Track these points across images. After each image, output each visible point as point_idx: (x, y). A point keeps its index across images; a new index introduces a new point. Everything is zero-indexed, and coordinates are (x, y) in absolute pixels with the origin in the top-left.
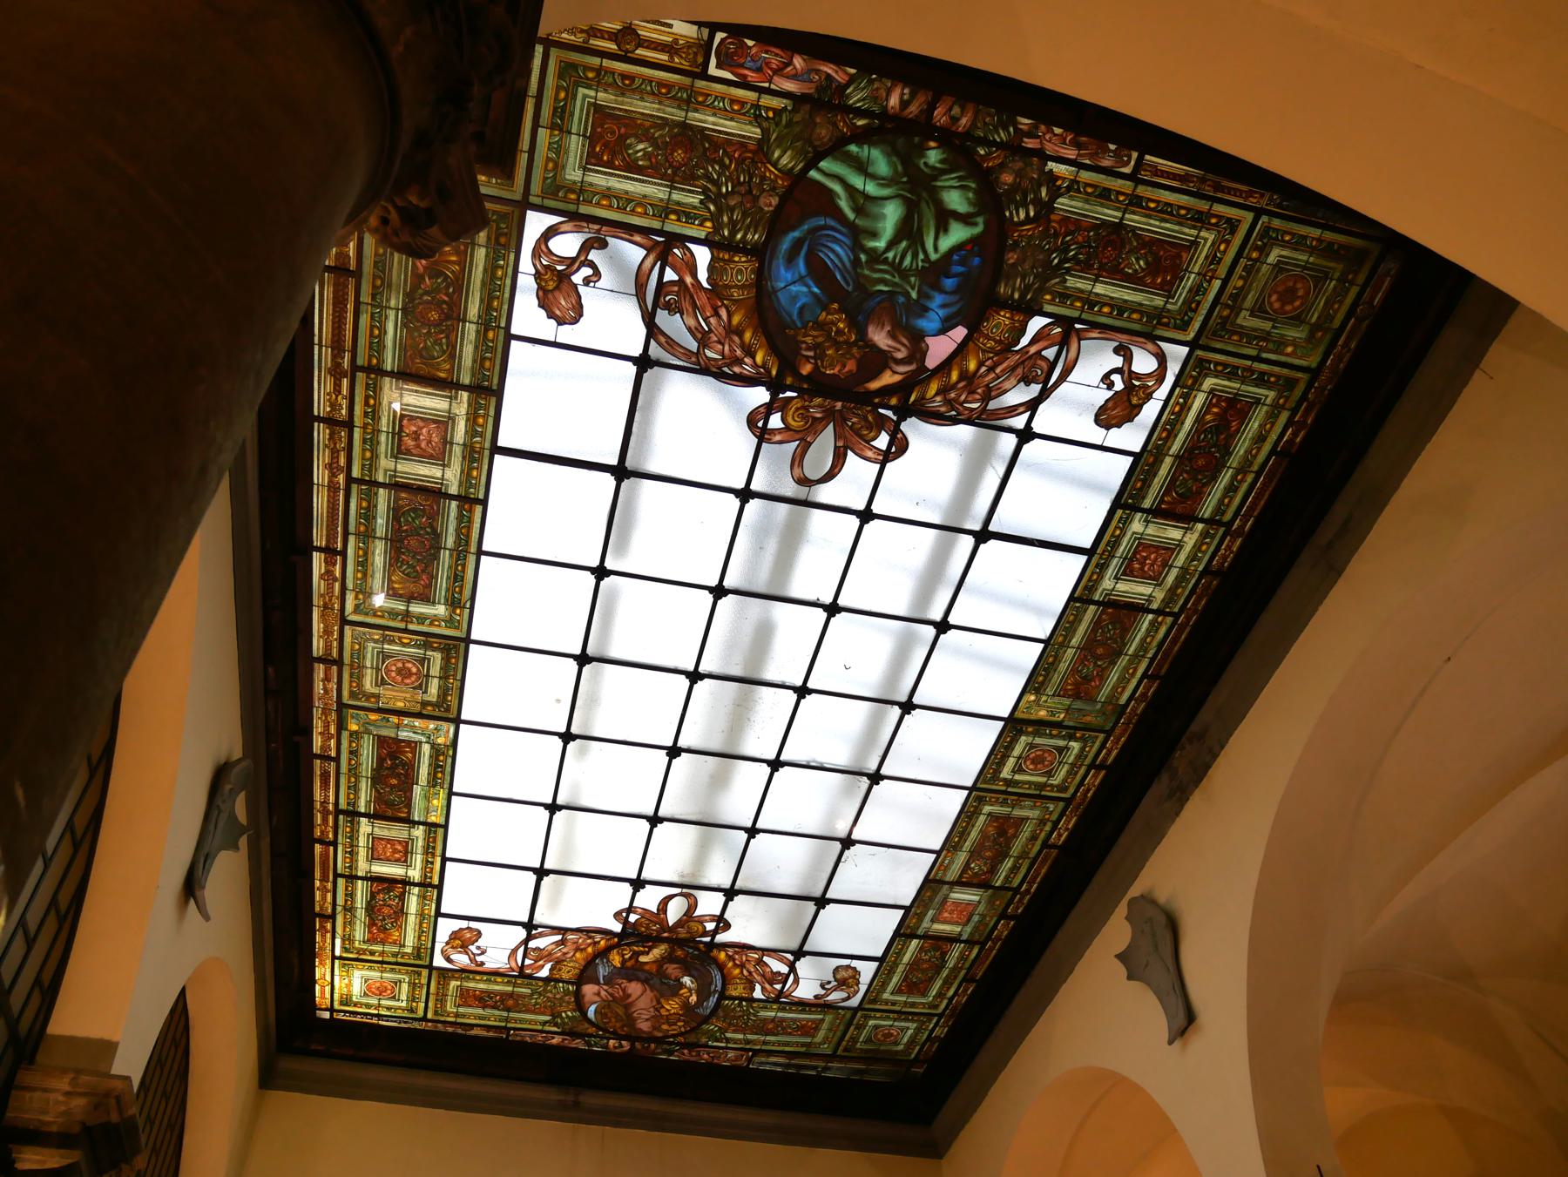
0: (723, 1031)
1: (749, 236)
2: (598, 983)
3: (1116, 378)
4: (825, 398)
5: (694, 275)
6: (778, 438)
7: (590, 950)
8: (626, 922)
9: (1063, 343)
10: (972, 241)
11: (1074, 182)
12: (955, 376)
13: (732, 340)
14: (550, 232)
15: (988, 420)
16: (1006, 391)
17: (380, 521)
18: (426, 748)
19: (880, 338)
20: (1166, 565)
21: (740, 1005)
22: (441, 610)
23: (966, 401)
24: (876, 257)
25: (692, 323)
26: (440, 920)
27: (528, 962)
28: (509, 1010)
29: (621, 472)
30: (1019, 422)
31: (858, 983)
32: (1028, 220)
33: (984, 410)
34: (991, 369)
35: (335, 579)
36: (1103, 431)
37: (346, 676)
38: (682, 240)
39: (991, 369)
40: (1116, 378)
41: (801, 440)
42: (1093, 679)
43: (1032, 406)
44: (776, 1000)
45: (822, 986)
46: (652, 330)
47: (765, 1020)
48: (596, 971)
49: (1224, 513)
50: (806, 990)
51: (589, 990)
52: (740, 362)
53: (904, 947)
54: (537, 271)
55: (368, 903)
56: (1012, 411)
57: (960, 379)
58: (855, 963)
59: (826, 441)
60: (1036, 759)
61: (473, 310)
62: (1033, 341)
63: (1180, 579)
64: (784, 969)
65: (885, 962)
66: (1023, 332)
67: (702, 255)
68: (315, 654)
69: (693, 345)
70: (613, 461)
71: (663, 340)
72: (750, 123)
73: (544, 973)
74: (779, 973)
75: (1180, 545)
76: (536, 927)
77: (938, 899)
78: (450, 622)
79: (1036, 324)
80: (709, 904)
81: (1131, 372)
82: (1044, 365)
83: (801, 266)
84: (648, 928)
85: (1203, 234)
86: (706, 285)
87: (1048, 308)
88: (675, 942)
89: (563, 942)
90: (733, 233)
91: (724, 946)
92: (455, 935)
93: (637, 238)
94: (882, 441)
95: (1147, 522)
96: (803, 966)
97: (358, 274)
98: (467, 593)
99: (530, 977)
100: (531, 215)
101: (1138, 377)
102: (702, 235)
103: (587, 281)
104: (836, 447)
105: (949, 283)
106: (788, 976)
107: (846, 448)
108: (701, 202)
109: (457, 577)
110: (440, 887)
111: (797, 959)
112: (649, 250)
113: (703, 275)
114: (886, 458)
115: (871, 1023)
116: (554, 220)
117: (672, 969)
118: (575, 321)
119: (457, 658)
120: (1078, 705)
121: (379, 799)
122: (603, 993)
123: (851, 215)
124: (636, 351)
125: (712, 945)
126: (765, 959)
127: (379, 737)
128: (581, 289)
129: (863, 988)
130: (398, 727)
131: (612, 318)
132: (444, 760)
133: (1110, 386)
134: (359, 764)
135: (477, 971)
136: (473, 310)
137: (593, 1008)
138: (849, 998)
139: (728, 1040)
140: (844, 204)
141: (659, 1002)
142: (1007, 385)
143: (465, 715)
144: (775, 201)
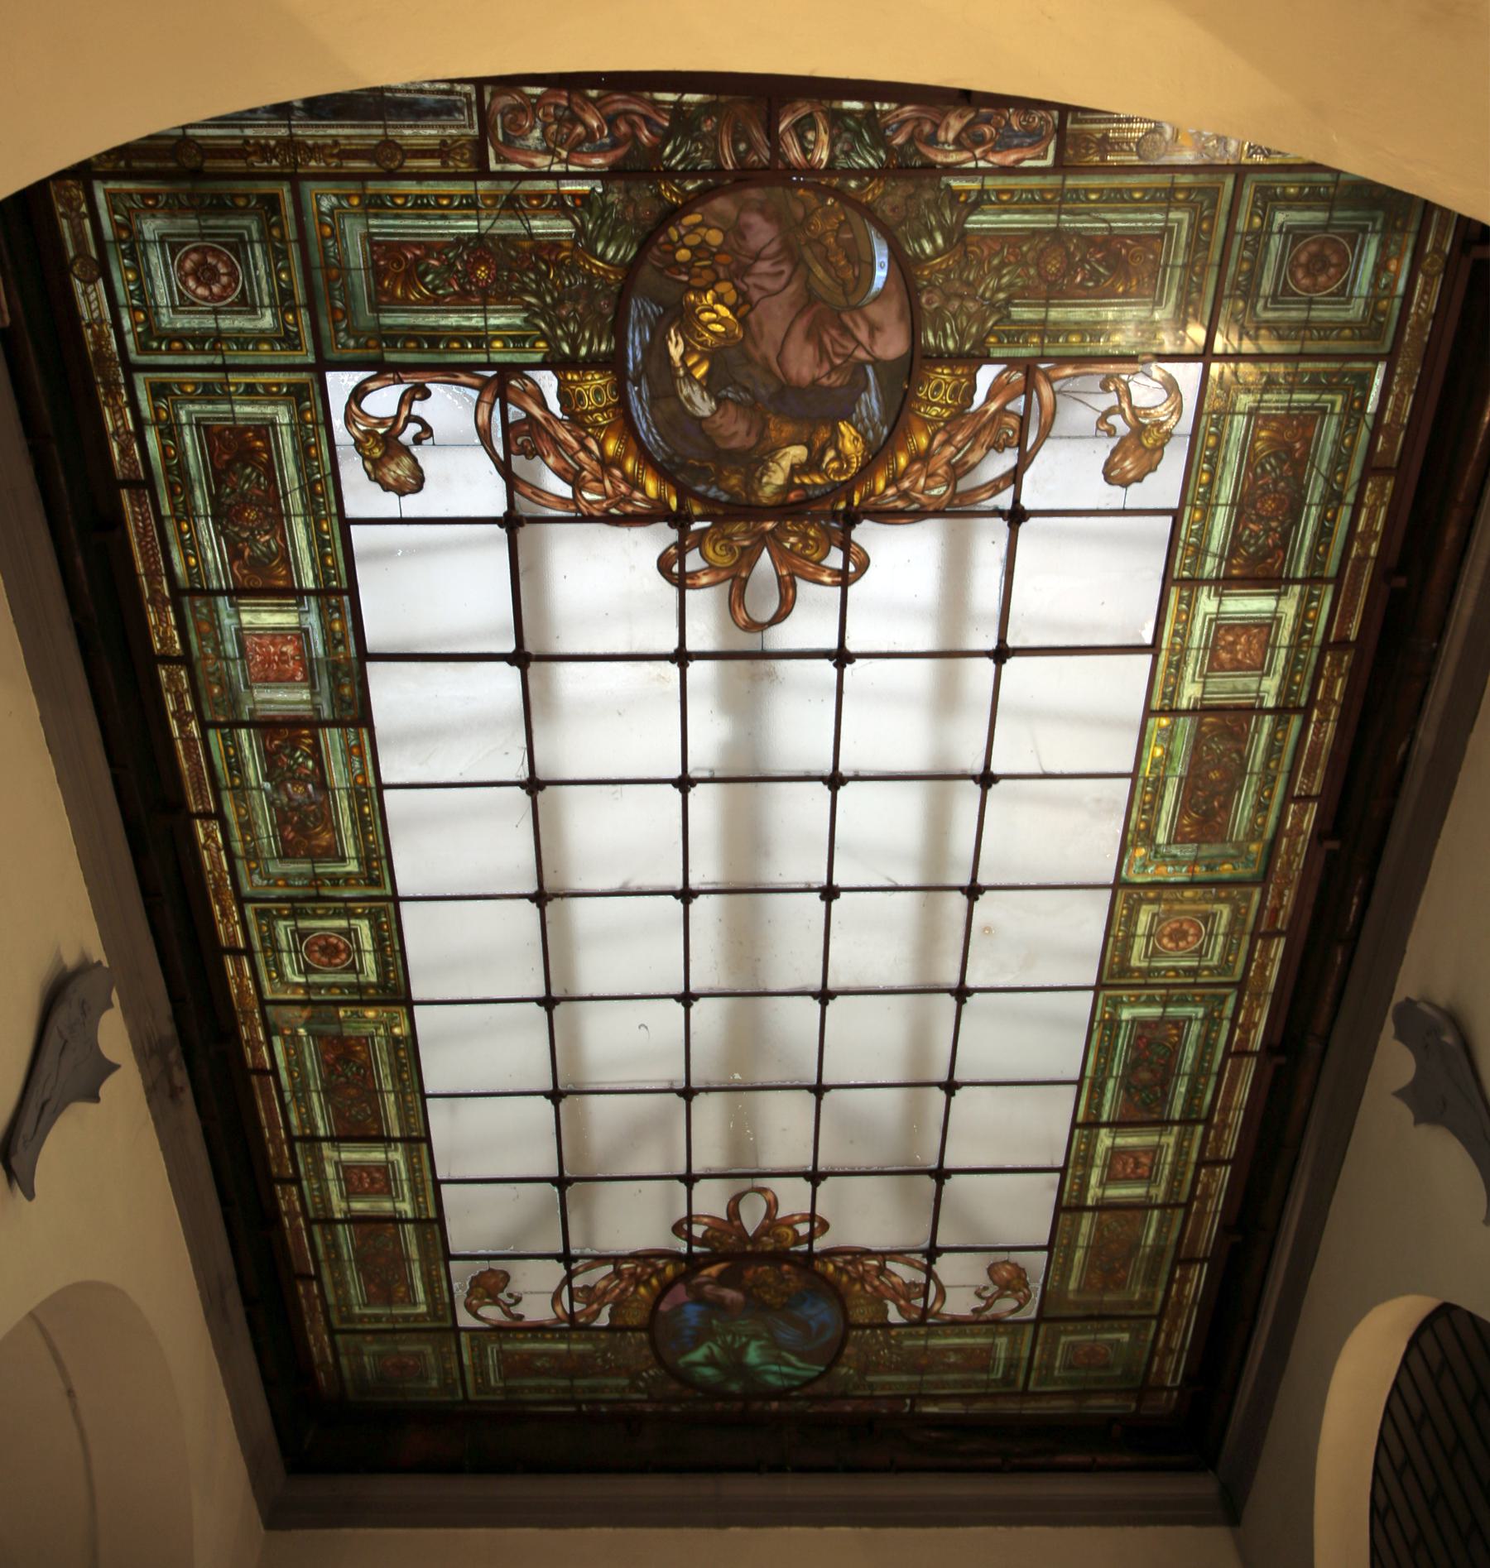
0: (583, 241)
2: (876, 362)
4: (748, 522)
5: (543, 404)
6: (704, 580)
7: (903, 461)
8: (846, 545)
9: (1029, 387)
10: (684, 1353)
13: (611, 475)
14: (359, 393)
15: (958, 508)
16: (974, 466)
17: (1183, 1090)
18: (1161, 837)
20: (1269, 645)
21: (875, 1336)
22: (1126, 1014)
25: (894, 1279)
26: (1175, 504)
30: (1004, 500)
32: (938, 253)
33: (954, 494)
35: (1242, 1026)
36: (1118, 489)
37: (1251, 919)
38: (518, 369)
40: (1115, 420)
42: (337, 1059)
43: (1015, 477)
44: (921, 1322)
45: (978, 1295)
49: (1323, 565)
51: (892, 345)
52: (847, 1262)
53: (1076, 1226)
54: (356, 439)
55: (1297, 521)
56: (995, 487)
57: (911, 462)
58: (1015, 1257)
60: (333, 951)
62: (990, 397)
63: (1292, 664)
64: (921, 1278)
65: (1057, 1244)
66: (973, 388)
67: (548, 382)
68: (1283, 941)
69: (566, 491)
70: (510, 647)
71: (528, 491)
74: (914, 1284)
75: (1276, 618)
76: (576, 1259)
78: (1117, 1003)
79: (986, 376)
80: (793, 1197)
81: (1133, 408)
82: (1014, 422)
83: (813, 1324)
84: (804, 537)
85: (1172, 215)
86: (560, 415)
87: (997, 353)
88: (743, 510)
89: (618, 1273)
90: (575, 348)
91: (830, 1253)
92: (476, 1282)
93: (463, 378)
95: (1220, 595)
96: (945, 1266)
97: (149, 483)
98: (1096, 1036)
99: (586, 1327)
100: (330, 376)
103: (418, 440)
105: (688, 1332)
106: (927, 1286)
107: (792, 575)
108: (526, 320)
109: (1106, 1052)
110: (1167, 580)
111: (932, 1261)
112: (481, 390)
113: (554, 406)
114: (844, 580)
116: (358, 376)
117: (736, 431)
119: (1112, 963)
120: (1207, 850)
121: (338, 1115)
122: (862, 335)
123: (784, 1354)
124: (499, 508)
125: (810, 1255)
126: (890, 1265)
127: (1223, 841)
130: (1196, 861)
132: (407, 1052)
133: (1111, 431)
134: (1259, 792)
135: (517, 1328)
138: (1020, 1307)
139: (871, 1386)
140: (793, 1359)
141: (743, 321)
143: (416, 994)
144: (847, 1351)
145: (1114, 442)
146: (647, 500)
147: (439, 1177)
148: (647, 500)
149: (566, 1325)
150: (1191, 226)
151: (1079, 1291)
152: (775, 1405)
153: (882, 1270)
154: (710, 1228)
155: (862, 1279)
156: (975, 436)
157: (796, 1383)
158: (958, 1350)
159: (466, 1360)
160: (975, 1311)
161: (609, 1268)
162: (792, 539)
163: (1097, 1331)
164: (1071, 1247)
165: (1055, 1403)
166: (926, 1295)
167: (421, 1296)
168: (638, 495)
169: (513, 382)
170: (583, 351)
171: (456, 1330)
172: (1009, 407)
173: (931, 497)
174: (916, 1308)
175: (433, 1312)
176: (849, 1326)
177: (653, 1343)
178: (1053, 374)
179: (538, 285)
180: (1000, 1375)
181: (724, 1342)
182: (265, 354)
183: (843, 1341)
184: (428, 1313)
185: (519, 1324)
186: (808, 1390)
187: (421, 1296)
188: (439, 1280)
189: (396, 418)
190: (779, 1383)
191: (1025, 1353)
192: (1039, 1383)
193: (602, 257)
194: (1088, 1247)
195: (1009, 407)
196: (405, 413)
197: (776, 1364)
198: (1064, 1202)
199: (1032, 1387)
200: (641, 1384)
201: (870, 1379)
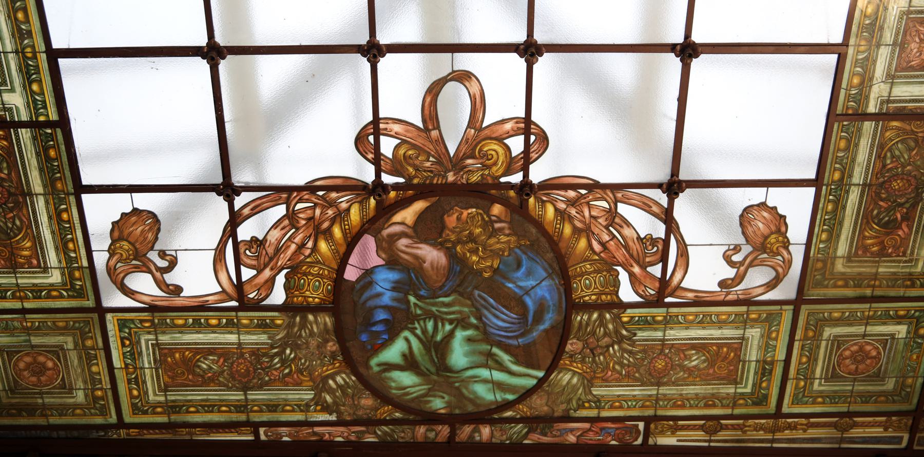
5: (632, 275)
6: (508, 126)
9: (239, 286)
10: (378, 349)
12: (337, 232)
13: (584, 222)
19: (431, 255)
21: (602, 321)
24: (462, 323)
25: (627, 232)
31: (786, 244)
39: (302, 246)
41: (481, 129)
43: (235, 219)
44: (657, 302)
50: (705, 272)
52: (572, 203)
54: (787, 248)
61: (854, 196)
64: (659, 230)
65: (826, 181)
67: (627, 294)
71: (655, 209)
83: (529, 301)
89: (291, 216)
90: (601, 317)
91: (549, 185)
92: (119, 229)
99: (257, 306)
101: (137, 269)
103: (737, 249)
105: (381, 315)
106: (666, 242)
107: (426, 130)
108: (635, 335)
113: (624, 276)
114: (376, 126)
123: (495, 350)
125: (526, 187)
133: (163, 254)
136: (854, 196)
139: (598, 402)
140: (505, 358)
142: (276, 234)
144: (569, 347)
145: (158, 246)
146: (553, 202)
147: (56, 45)
148: (553, 202)
149: (234, 303)
150: (146, 393)
151: (849, 258)
152: (486, 431)
153: (612, 215)
154: (404, 142)
155: (586, 231)
156: (278, 251)
157: (510, 397)
158: (700, 347)
159: (117, 362)
160: (722, 284)
161: (281, 210)
162: (428, 164)
163: (867, 321)
164: (843, 186)
165: (813, 433)
166: (664, 259)
167: (52, 257)
168: (562, 206)
169: (652, 292)
170: (595, 316)
171: (101, 311)
172: (254, 272)
173: (307, 201)
174: (652, 277)
175: (70, 286)
176: (571, 306)
177: (339, 332)
178: (223, 297)
179: (622, 356)
180: (748, 390)
181: (424, 331)
182: (836, 310)
183: (564, 330)
184: (64, 284)
185: (177, 302)
186: (524, 409)
187: (52, 257)
188: (72, 229)
189: (751, 265)
190: (490, 397)
191: (781, 355)
192: (796, 401)
193: (575, 373)
194: (864, 185)
195: (254, 272)
196: (742, 268)
197: (486, 366)
198: (839, 109)
199: (785, 409)
200: (329, 399)
201: (596, 391)
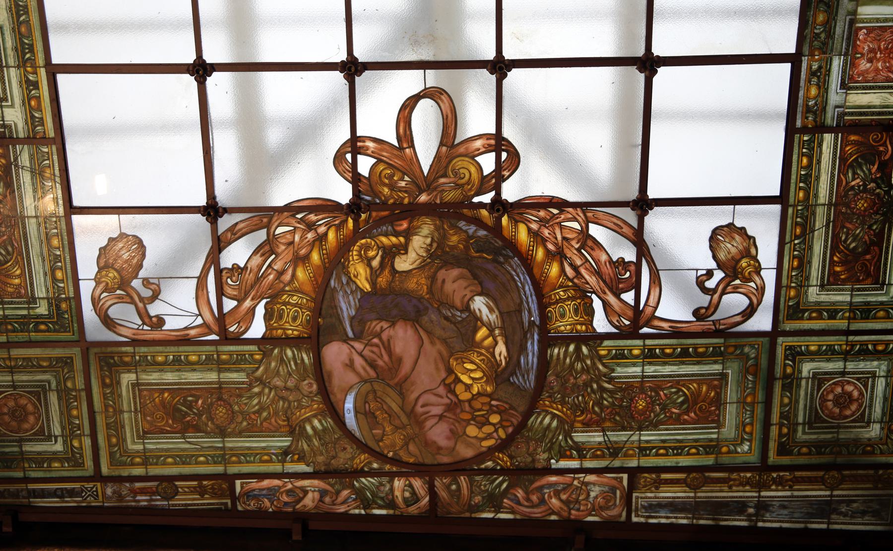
1: (563, 351)
3: (147, 293)
5: (606, 305)
6: (478, 144)
7: (315, 257)
8: (355, 179)
9: (221, 318)
11: (283, 461)
12: (315, 257)
13: (556, 244)
14: (750, 312)
16: (255, 252)
23: (293, 232)
27: (229, 305)
28: (222, 433)
29: (649, 64)
30: (225, 223)
32: (309, 420)
33: (268, 226)
34: (281, 273)
46: (638, 238)
47: (629, 389)
48: (335, 307)
51: (335, 353)
52: (543, 222)
54: (758, 273)
57: (307, 257)
59: (426, 150)
62: (252, 311)
64: (629, 254)
66: (268, 317)
72: (583, 443)
73: (257, 329)
74: (622, 262)
77: (840, 28)
82: (228, 291)
86: (594, 296)
94: (365, 165)
102: (607, 343)
104: (412, 146)
106: (638, 265)
112: (653, 317)
113: (597, 304)
115: (807, 368)
118: (715, 232)
122: (359, 361)
128: (713, 265)
129: (769, 277)
131: (683, 241)
137: (349, 405)
139: (581, 451)
141: (450, 371)
142: (257, 260)
